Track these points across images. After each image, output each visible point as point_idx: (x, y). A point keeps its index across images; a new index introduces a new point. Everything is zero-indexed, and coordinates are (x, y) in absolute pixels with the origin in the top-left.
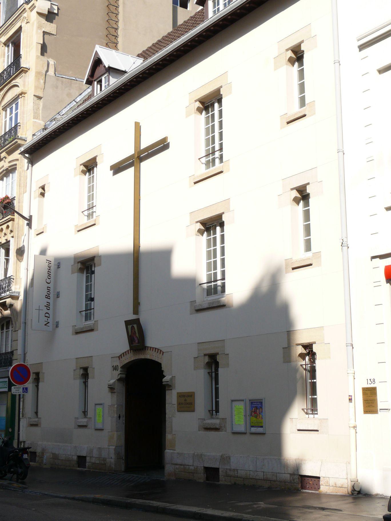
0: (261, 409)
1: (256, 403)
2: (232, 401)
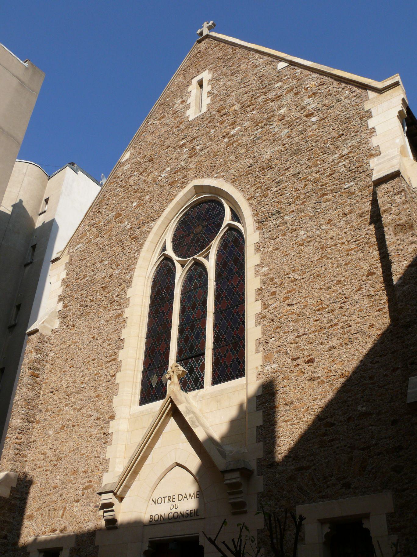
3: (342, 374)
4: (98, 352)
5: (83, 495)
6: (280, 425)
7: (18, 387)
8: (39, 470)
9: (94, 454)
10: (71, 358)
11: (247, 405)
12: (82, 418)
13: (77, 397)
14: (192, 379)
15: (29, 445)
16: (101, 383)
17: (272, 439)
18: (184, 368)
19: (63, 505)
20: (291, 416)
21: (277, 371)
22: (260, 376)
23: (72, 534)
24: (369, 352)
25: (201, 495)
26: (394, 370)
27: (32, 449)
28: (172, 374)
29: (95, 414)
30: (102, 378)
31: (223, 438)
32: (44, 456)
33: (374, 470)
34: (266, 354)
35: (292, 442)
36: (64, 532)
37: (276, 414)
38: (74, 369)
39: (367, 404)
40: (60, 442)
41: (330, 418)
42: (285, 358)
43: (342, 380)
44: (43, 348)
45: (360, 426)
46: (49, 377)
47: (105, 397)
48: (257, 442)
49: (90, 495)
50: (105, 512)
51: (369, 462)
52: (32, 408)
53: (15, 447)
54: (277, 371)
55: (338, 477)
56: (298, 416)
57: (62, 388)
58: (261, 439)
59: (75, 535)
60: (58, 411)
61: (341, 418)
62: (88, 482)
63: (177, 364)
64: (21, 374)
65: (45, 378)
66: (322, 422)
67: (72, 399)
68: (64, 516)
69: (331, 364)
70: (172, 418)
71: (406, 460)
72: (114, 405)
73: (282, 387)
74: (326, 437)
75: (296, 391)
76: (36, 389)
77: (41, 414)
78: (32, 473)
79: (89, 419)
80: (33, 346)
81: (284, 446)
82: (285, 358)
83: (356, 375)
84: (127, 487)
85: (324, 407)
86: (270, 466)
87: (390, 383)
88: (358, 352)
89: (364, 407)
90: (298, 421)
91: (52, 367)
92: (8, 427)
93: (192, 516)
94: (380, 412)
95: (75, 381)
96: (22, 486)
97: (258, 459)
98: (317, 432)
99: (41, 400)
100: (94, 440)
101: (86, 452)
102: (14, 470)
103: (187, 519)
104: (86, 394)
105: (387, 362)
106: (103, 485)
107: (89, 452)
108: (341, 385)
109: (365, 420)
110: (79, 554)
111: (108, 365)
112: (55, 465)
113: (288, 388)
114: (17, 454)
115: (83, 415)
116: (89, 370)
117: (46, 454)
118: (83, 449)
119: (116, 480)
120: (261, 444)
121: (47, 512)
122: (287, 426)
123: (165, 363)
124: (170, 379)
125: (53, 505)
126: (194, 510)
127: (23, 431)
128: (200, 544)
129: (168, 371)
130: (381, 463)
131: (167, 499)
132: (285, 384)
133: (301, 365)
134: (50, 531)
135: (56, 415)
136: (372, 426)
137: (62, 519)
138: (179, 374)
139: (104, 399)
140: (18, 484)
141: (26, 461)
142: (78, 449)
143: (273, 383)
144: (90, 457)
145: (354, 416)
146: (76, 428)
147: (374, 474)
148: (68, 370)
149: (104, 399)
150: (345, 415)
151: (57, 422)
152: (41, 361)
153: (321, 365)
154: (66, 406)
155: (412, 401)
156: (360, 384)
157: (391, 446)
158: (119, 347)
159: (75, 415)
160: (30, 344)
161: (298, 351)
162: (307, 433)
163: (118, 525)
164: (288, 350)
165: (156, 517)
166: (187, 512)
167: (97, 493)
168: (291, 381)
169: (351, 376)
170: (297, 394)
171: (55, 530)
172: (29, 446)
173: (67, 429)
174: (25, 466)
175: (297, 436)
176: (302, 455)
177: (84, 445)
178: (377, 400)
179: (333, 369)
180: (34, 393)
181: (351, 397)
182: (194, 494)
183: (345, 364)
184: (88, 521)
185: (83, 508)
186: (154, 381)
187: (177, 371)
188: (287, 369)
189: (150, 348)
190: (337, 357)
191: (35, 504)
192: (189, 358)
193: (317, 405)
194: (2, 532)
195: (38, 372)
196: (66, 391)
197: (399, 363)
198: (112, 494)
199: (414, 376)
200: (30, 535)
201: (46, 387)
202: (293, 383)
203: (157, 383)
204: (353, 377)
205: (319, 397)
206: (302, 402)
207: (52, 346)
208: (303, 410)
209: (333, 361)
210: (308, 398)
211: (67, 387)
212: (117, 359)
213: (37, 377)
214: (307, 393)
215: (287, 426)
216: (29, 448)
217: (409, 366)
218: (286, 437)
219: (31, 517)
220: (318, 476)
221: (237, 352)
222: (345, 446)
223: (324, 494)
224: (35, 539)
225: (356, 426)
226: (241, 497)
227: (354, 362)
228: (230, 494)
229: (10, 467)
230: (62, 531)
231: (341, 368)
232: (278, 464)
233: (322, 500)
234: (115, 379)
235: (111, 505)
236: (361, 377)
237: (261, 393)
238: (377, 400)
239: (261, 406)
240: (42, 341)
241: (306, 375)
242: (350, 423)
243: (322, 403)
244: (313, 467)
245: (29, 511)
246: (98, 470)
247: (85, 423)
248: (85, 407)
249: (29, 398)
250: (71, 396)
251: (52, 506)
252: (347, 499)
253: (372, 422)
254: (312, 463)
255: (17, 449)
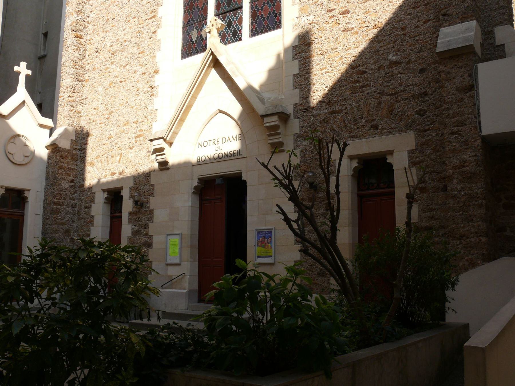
0: (270, 238)
1: (264, 233)
2: (168, 235)
3: (375, 25)
4: (138, 10)
5: (136, 142)
6: (315, 73)
7: (64, 49)
8: (94, 123)
9: (142, 106)
10: (112, 18)
11: (283, 55)
12: (128, 74)
13: (121, 54)
14: (231, 32)
15: (81, 102)
16: (143, 40)
17: (307, 86)
18: (222, 21)
19: (120, 152)
20: (325, 64)
21: (312, 22)
22: (296, 27)
23: (130, 175)
24: (402, 4)
25: (243, 137)
26: (426, 22)
27: (85, 106)
28: (211, 27)
29: (141, 70)
30: (144, 35)
31: (262, 86)
32: (96, 111)
33: (400, 114)
34: (302, 6)
35: (326, 89)
36: (123, 175)
37: (311, 63)
38: (116, 28)
39: (397, 54)
40: (110, 98)
41: (362, 66)
42: (321, 9)
43: (375, 31)
44: (83, 9)
45: (389, 74)
46: (93, 38)
47: (148, 53)
48: (293, 89)
49: (142, 142)
50: (157, 156)
51: (396, 106)
52: (79, 68)
53: (69, 104)
54: (312, 22)
55: (367, 119)
56: (332, 65)
57: (107, 48)
58: (297, 86)
59: (132, 176)
60: (105, 69)
61: (373, 67)
62: (139, 131)
63: (216, 18)
64: (65, 36)
65: (88, 38)
66: (354, 70)
67: (117, 57)
68: (121, 162)
69: (365, 15)
70: (213, 69)
71: (430, 105)
72: (157, 60)
73: (317, 37)
74: (357, 84)
75: (330, 42)
76: (82, 50)
77: (90, 73)
78: (87, 127)
79: (135, 74)
80: (72, 8)
81: (318, 92)
82: (321, 9)
83: (388, 26)
84: (175, 133)
85: (356, 57)
86: (305, 110)
87: (420, 34)
88: (392, 3)
89: (395, 56)
90: (332, 69)
91: (94, 27)
92: (60, 87)
93: (235, 156)
94: (409, 61)
95: (118, 40)
96: (80, 138)
97: (294, 105)
98: (349, 80)
99: (88, 59)
100: (141, 93)
101: (134, 104)
102: (71, 125)
103: (231, 158)
104: (130, 52)
105: (420, 14)
106: (153, 133)
107: (137, 104)
108: (373, 35)
109: (395, 68)
110: (138, 191)
111: (149, 22)
112: (107, 119)
113: (323, 38)
114: (71, 111)
115: (129, 71)
116: (131, 28)
117: (98, 109)
118: (132, 103)
119: (165, 128)
120: (297, 90)
121: (106, 159)
122: (322, 74)
123: (204, 17)
124: (209, 32)
125: (110, 153)
126: (236, 151)
127: (74, 89)
128: (243, 179)
129: (207, 25)
130: (407, 107)
131: (212, 142)
132: (320, 35)
133: (336, 16)
134: (110, 174)
135: (104, 73)
136: (401, 74)
137: (119, 164)
138: (218, 28)
139: (147, 55)
140: (76, 136)
141: (81, 116)
142: (127, 102)
143: (309, 34)
144: (139, 109)
145: (384, 65)
146: (123, 83)
147: (400, 117)
148: (110, 30)
149: (147, 55)
150: (376, 64)
151: (105, 79)
152: (84, 22)
153: (355, 16)
154: (112, 63)
155: (441, 50)
156: (392, 34)
157: (417, 92)
158: (158, 4)
159: (121, 71)
160: (70, 5)
161: (334, 3)
162: (340, 80)
163: (169, 166)
164: (323, 2)
165: (203, 159)
166: (231, 152)
167: (149, 140)
168: (326, 32)
169: (384, 27)
170: (331, 44)
171: (115, 174)
172: (82, 103)
173: (115, 85)
174: (80, 121)
175: (331, 83)
176: (335, 100)
177: (133, 99)
178: (408, 50)
179: (367, 20)
180: (80, 53)
181: (383, 47)
182: (236, 137)
183: (379, 16)
184: (143, 164)
185: (137, 153)
186: (194, 35)
187: (216, 24)
188: (322, 20)
189: (188, 4)
190: (371, 9)
191: (94, 152)
192: (226, 12)
193: (350, 54)
194: (69, 177)
195: (82, 34)
196: (111, 50)
197: (431, 15)
198: (162, 140)
199: (445, 27)
200: (93, 179)
201: (91, 48)
202: (328, 33)
203: (197, 38)
204: (385, 28)
205: (353, 47)
206: (336, 51)
207: (92, 7)
208: (336, 59)
209: (367, 12)
210: (342, 48)
211: (111, 46)
212: (157, 15)
213: (81, 38)
214: (341, 43)
215: (322, 74)
216: (82, 104)
217: (441, 17)
218: (320, 84)
219: (92, 164)
220: (349, 119)
221: (274, 5)
222: (375, 92)
223: (354, 134)
224: (99, 182)
225: (386, 74)
226: (279, 138)
227: (388, 14)
228: (269, 135)
229: (67, 122)
230: (120, 174)
231: (374, 19)
232: (313, 108)
233: (352, 139)
234: (156, 36)
235: (161, 150)
236: (394, 28)
237: (297, 44)
238: (408, 50)
239: (297, 55)
240: (81, 2)
241: (340, 26)
242: (380, 71)
243: (354, 53)
244: (345, 111)
245: (89, 159)
246: (148, 120)
247: (132, 78)
248: (130, 63)
249: (75, 58)
250: (115, 54)
251: (109, 153)
252: (375, 138)
253: (401, 70)
254: (344, 107)
255: (71, 106)
